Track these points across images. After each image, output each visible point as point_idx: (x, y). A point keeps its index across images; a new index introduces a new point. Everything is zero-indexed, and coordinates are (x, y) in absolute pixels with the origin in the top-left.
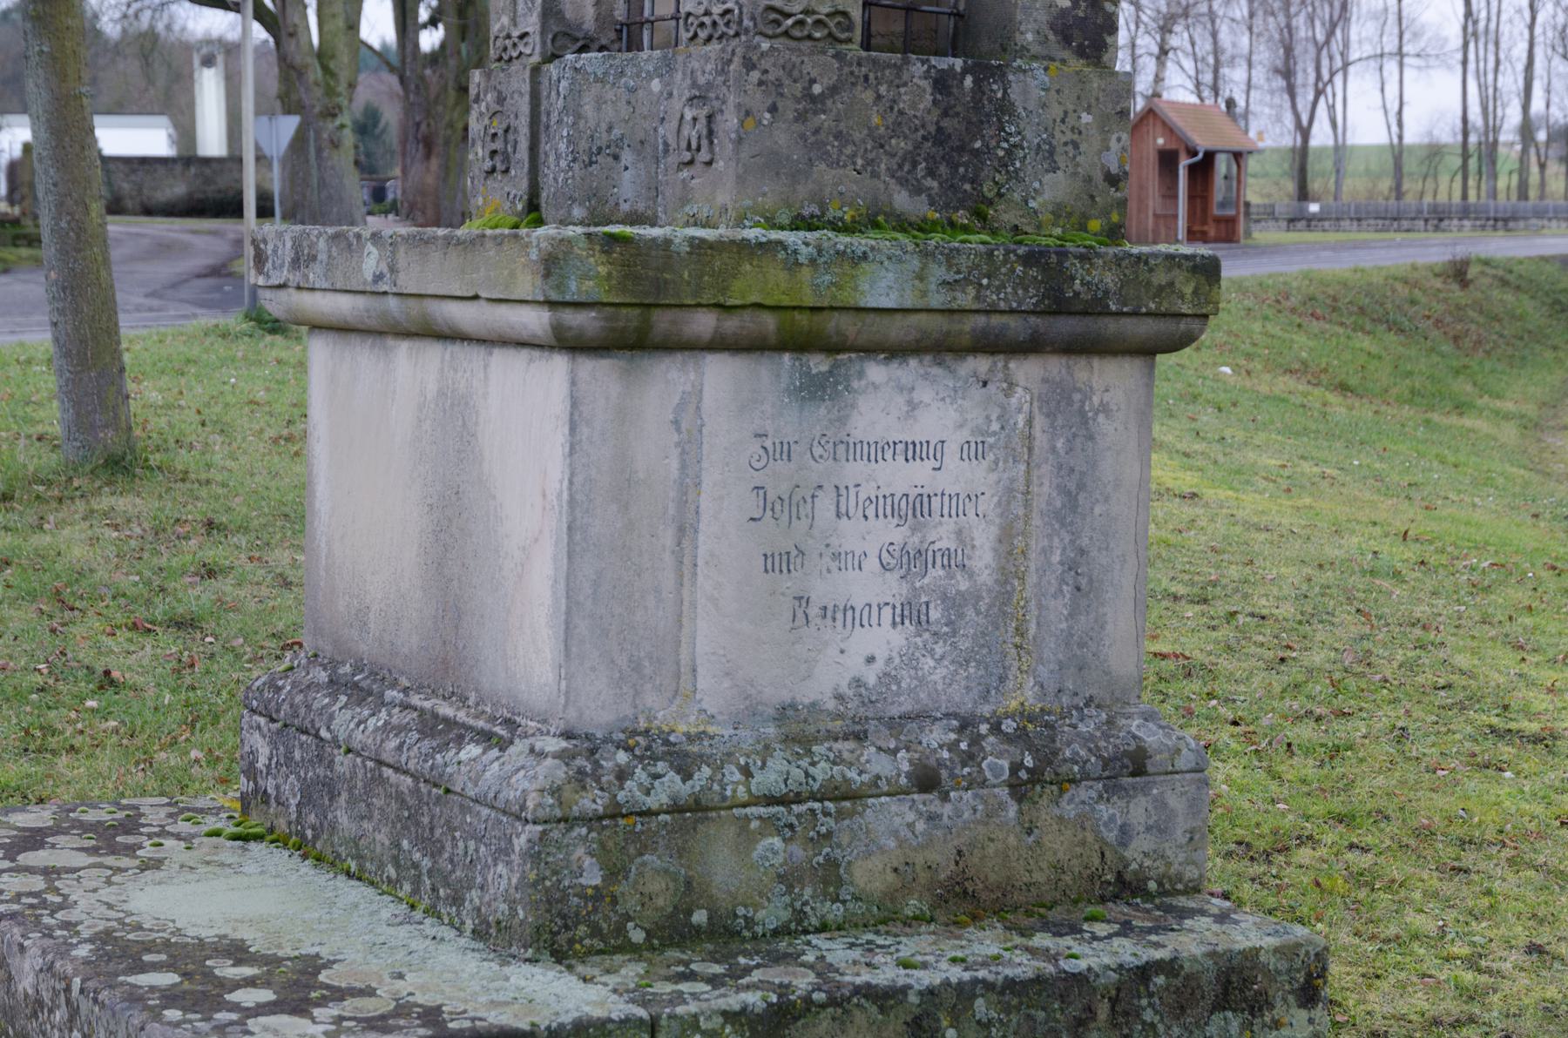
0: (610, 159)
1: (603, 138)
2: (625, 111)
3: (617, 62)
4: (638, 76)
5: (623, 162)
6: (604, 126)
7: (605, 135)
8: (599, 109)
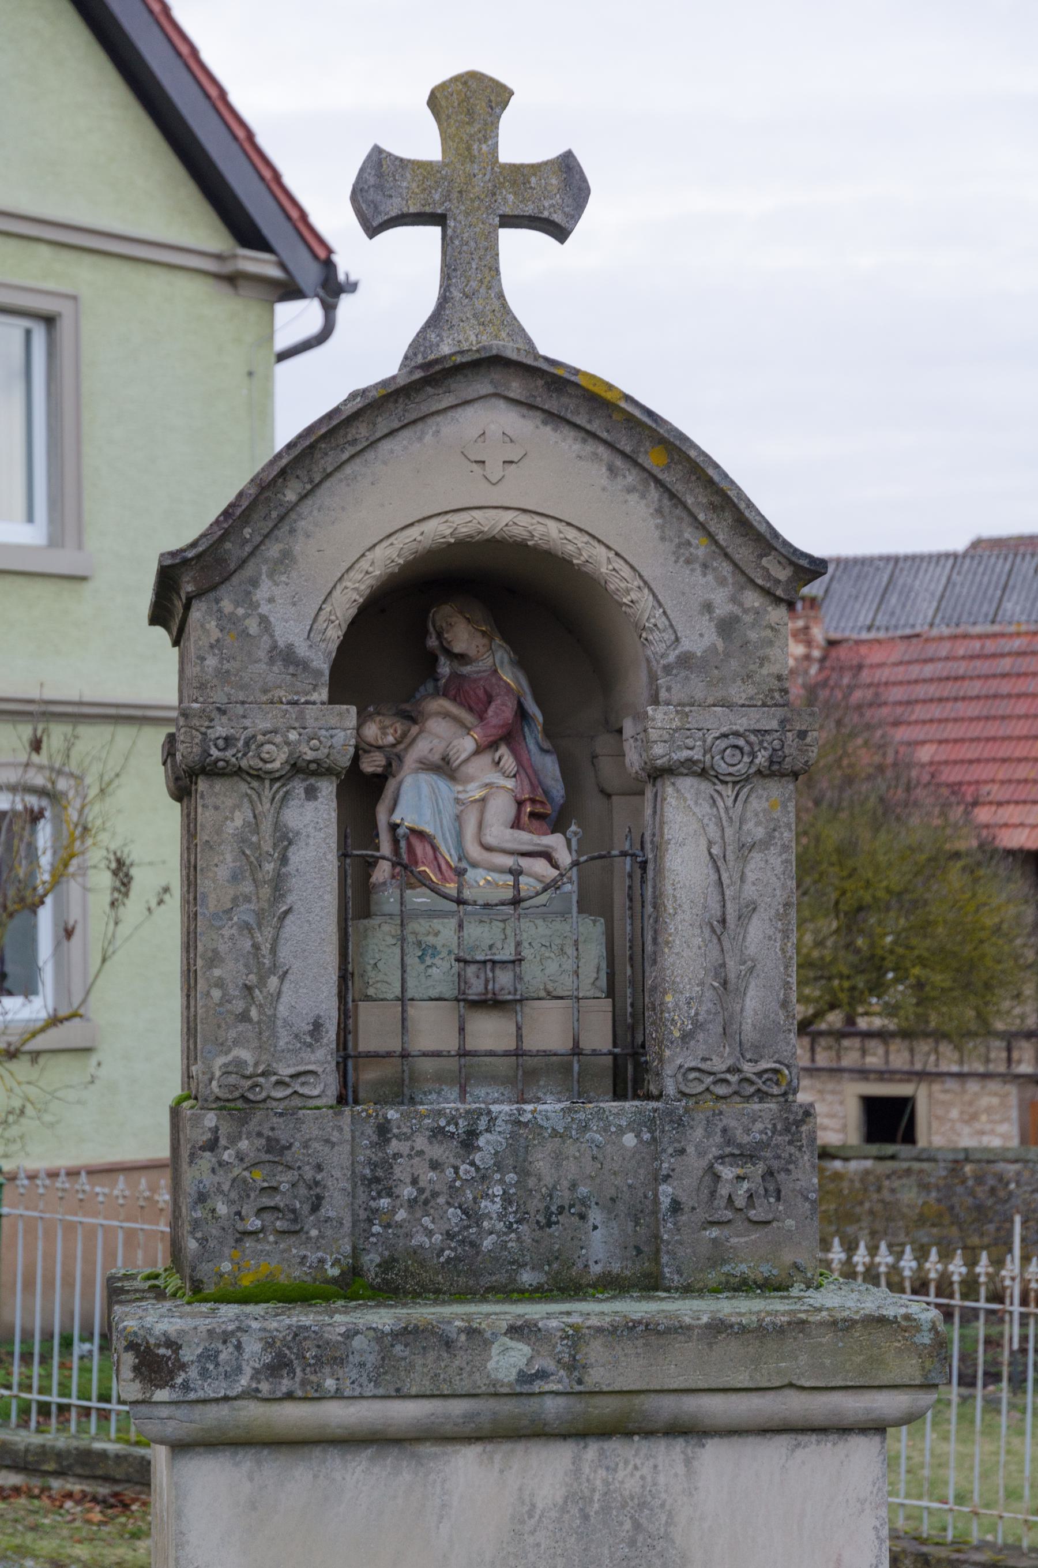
0: (575, 1219)
1: (564, 1196)
2: (590, 1168)
3: (581, 1116)
4: (606, 1129)
5: (591, 1221)
6: (565, 1184)
7: (566, 1193)
8: (559, 1165)
